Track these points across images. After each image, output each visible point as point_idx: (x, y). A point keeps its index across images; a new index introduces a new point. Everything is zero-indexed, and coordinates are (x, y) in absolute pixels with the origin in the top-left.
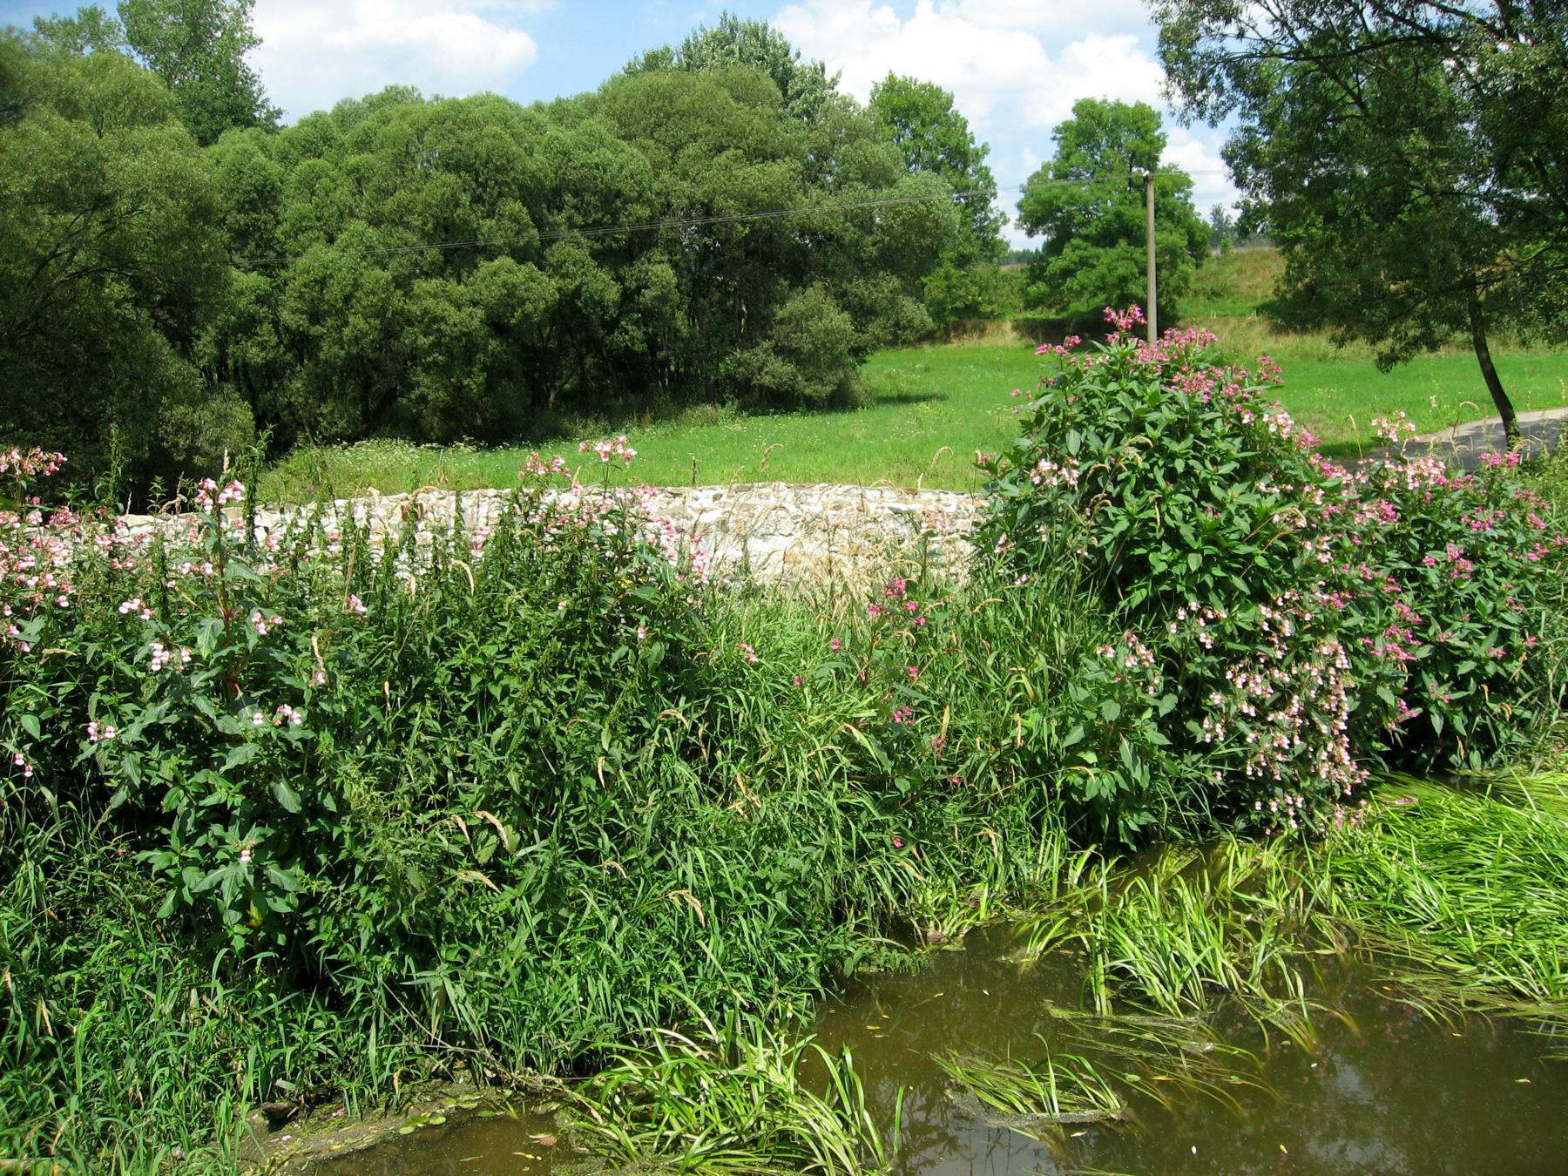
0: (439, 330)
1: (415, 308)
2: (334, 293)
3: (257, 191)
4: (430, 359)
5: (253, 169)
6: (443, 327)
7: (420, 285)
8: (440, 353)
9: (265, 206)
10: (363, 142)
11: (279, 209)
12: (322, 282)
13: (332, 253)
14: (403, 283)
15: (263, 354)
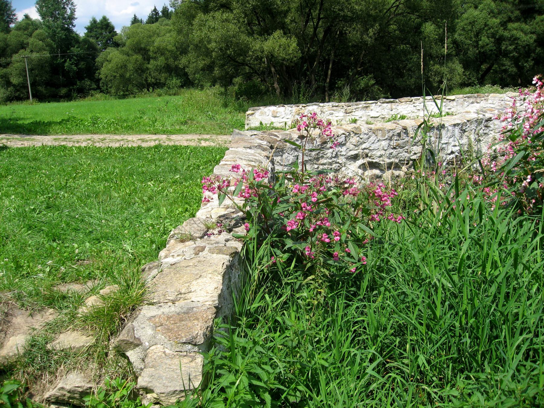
0: (517, 43)
1: (506, 34)
4: (512, 55)
6: (519, 42)
7: (510, 25)
8: (516, 52)
10: (204, 10)
13: (476, 13)
14: (504, 24)
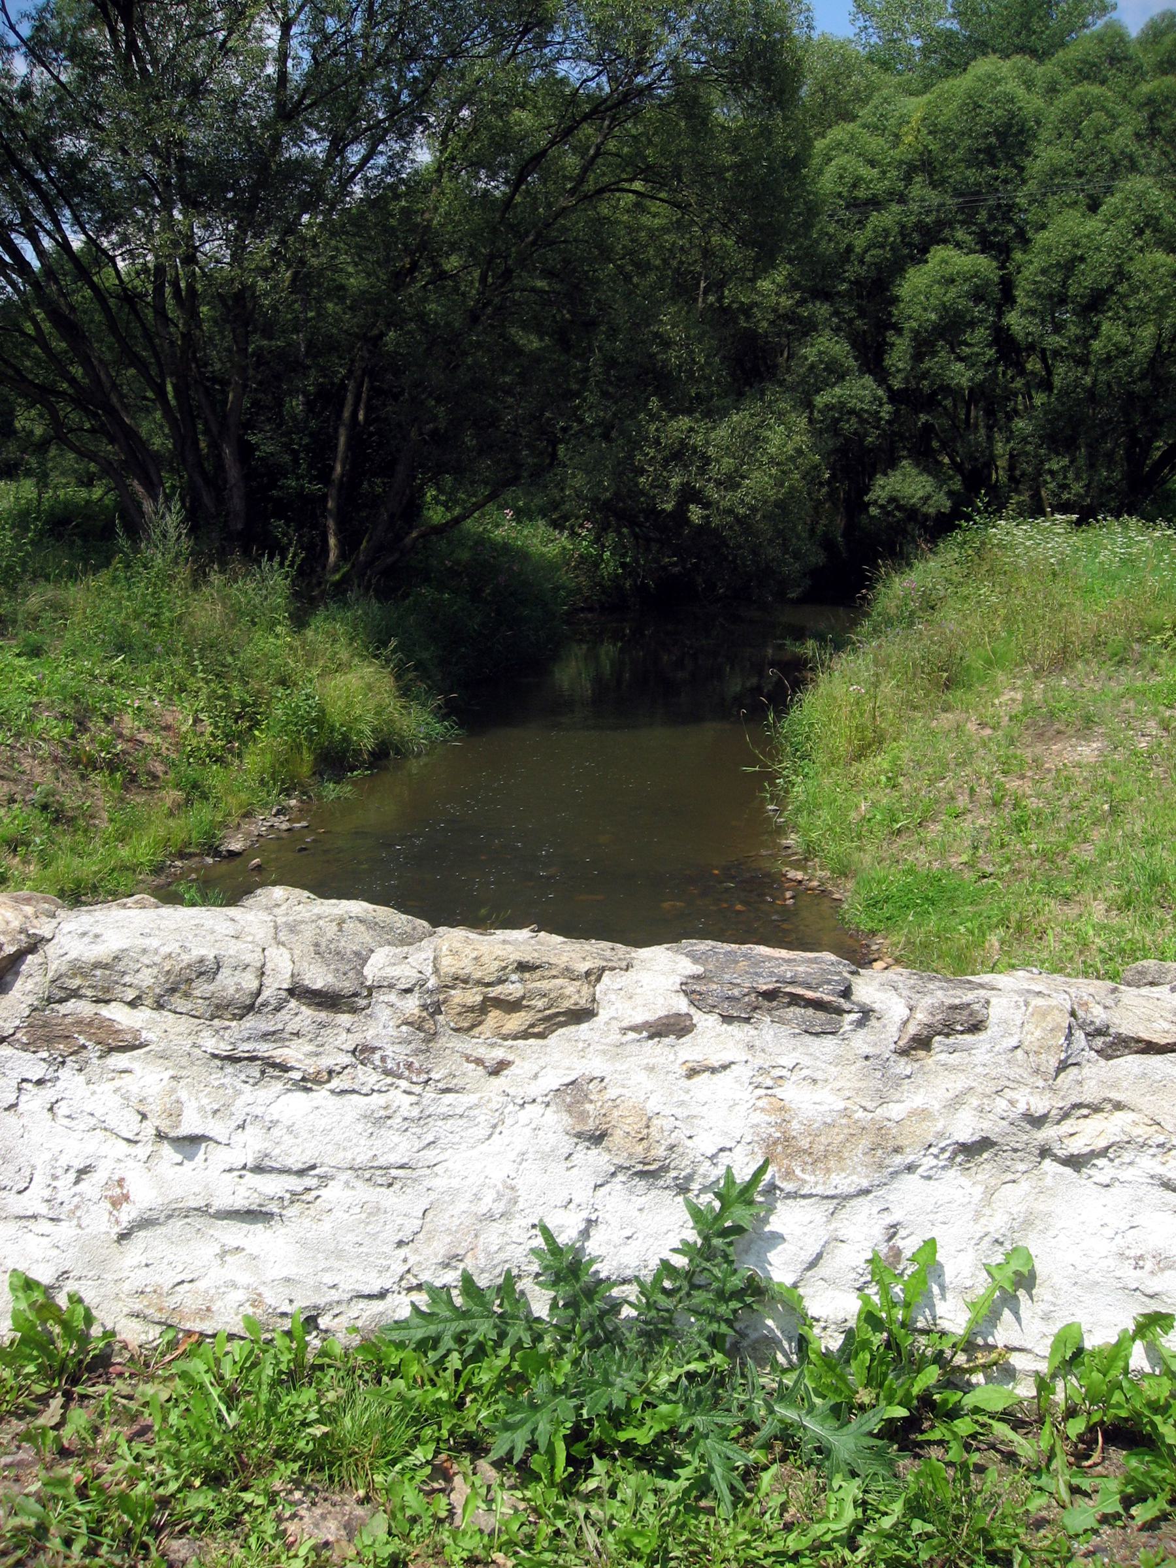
2: (1083, 283)
3: (997, 133)
5: (995, 101)
9: (1009, 157)
11: (1027, 162)
12: (1069, 266)
13: (1094, 224)
15: (970, 373)
